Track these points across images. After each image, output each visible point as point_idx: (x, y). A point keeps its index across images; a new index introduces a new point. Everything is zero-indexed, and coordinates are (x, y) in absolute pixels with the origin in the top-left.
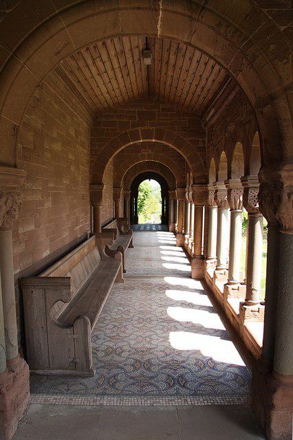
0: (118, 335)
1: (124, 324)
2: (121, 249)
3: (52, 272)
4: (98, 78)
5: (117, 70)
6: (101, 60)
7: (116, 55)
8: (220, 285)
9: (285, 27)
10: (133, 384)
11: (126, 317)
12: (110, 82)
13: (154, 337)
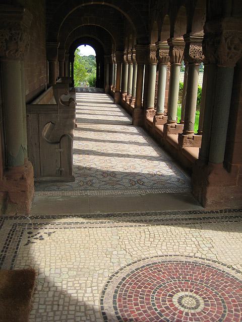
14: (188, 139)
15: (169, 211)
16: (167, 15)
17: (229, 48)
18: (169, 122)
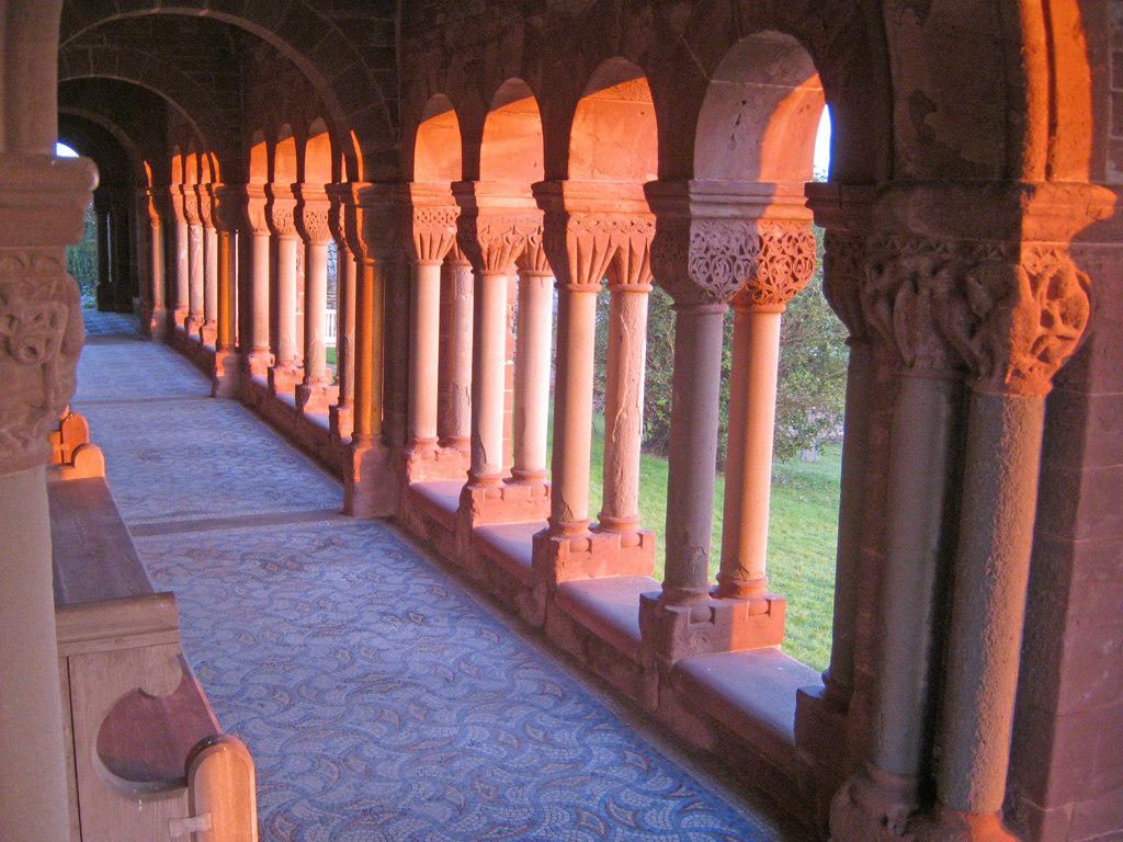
14: (694, 620)
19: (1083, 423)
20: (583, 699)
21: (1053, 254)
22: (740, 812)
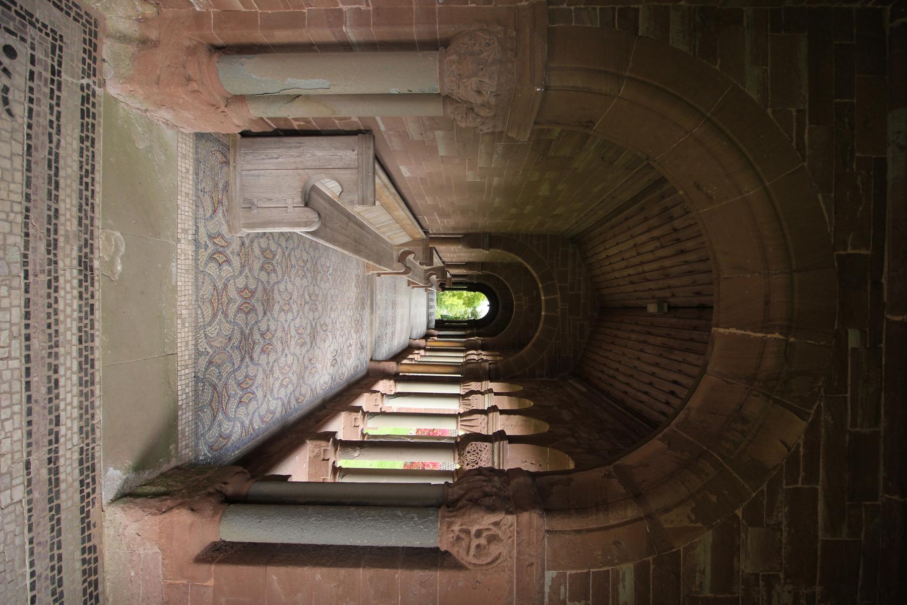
0: (293, 266)
1: (309, 275)
2: (407, 271)
3: (381, 178)
4: (631, 243)
5: (640, 269)
6: (657, 248)
7: (663, 268)
8: (365, 401)
9: (740, 516)
10: (215, 288)
11: (319, 278)
12: (623, 259)
13: (290, 316)
14: (325, 450)
15: (99, 416)
16: (532, 404)
17: (479, 534)
18: (364, 413)
19: (423, 568)
20: (296, 410)
21: (510, 537)
22: (237, 452)
